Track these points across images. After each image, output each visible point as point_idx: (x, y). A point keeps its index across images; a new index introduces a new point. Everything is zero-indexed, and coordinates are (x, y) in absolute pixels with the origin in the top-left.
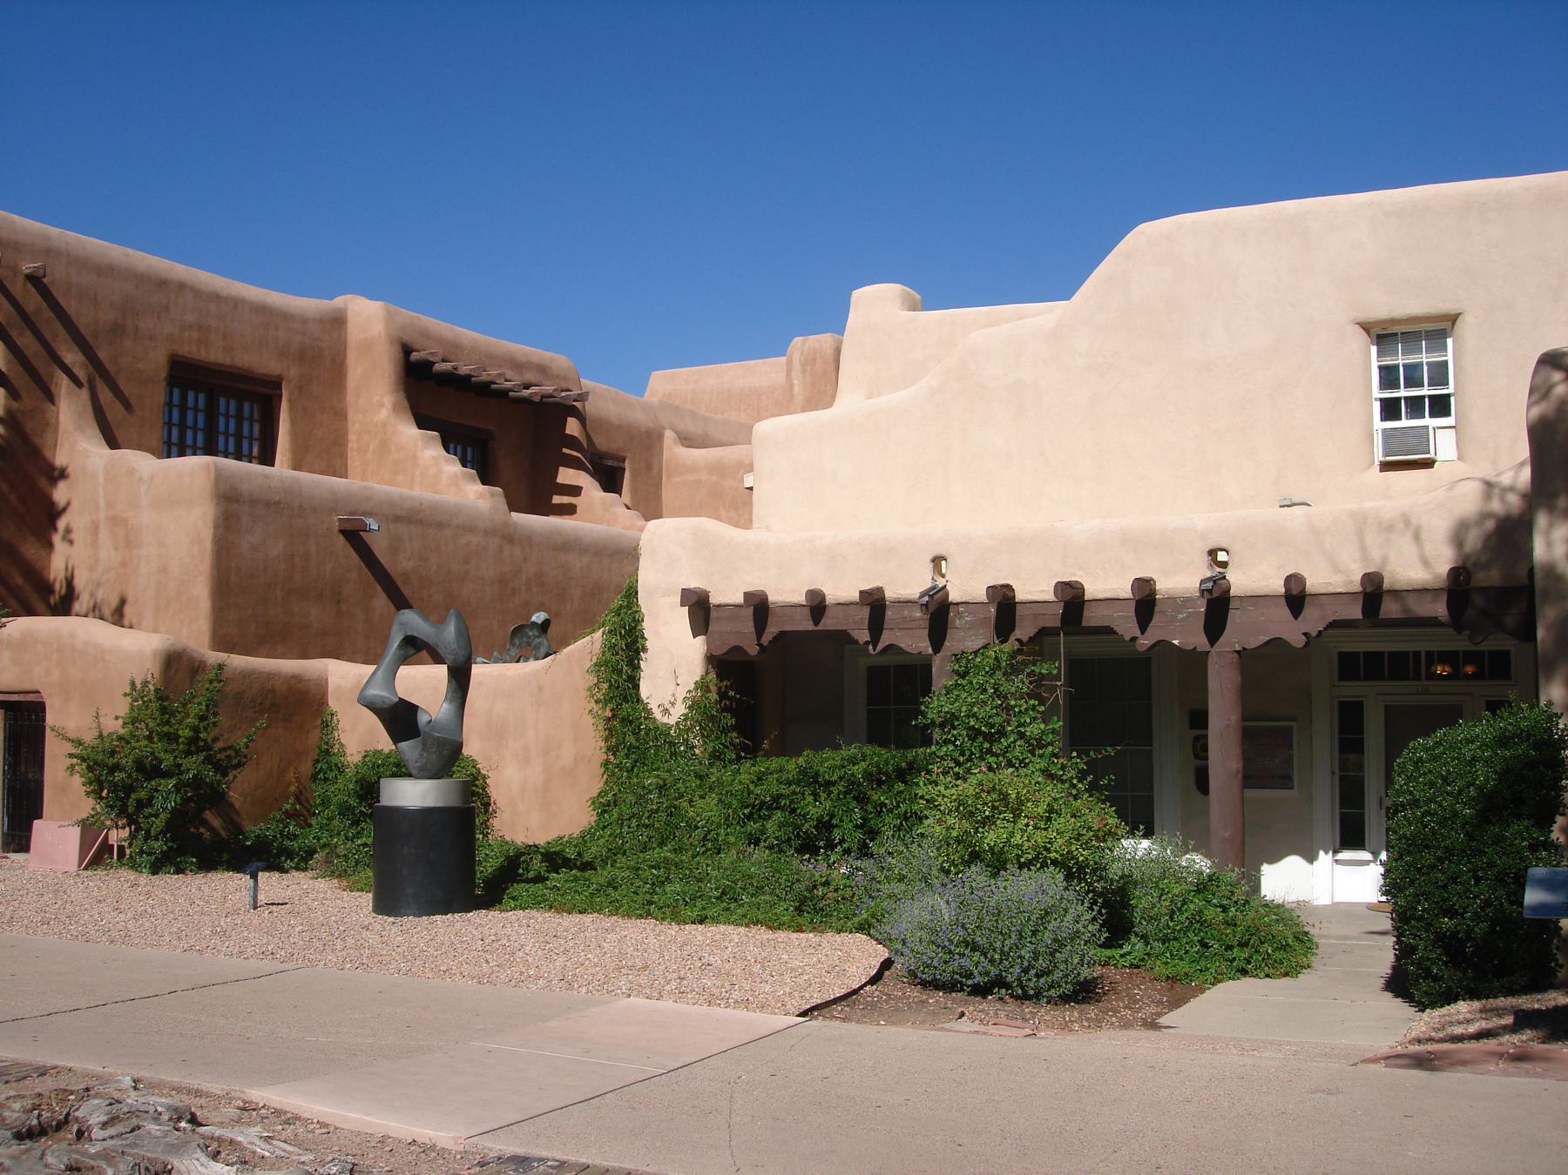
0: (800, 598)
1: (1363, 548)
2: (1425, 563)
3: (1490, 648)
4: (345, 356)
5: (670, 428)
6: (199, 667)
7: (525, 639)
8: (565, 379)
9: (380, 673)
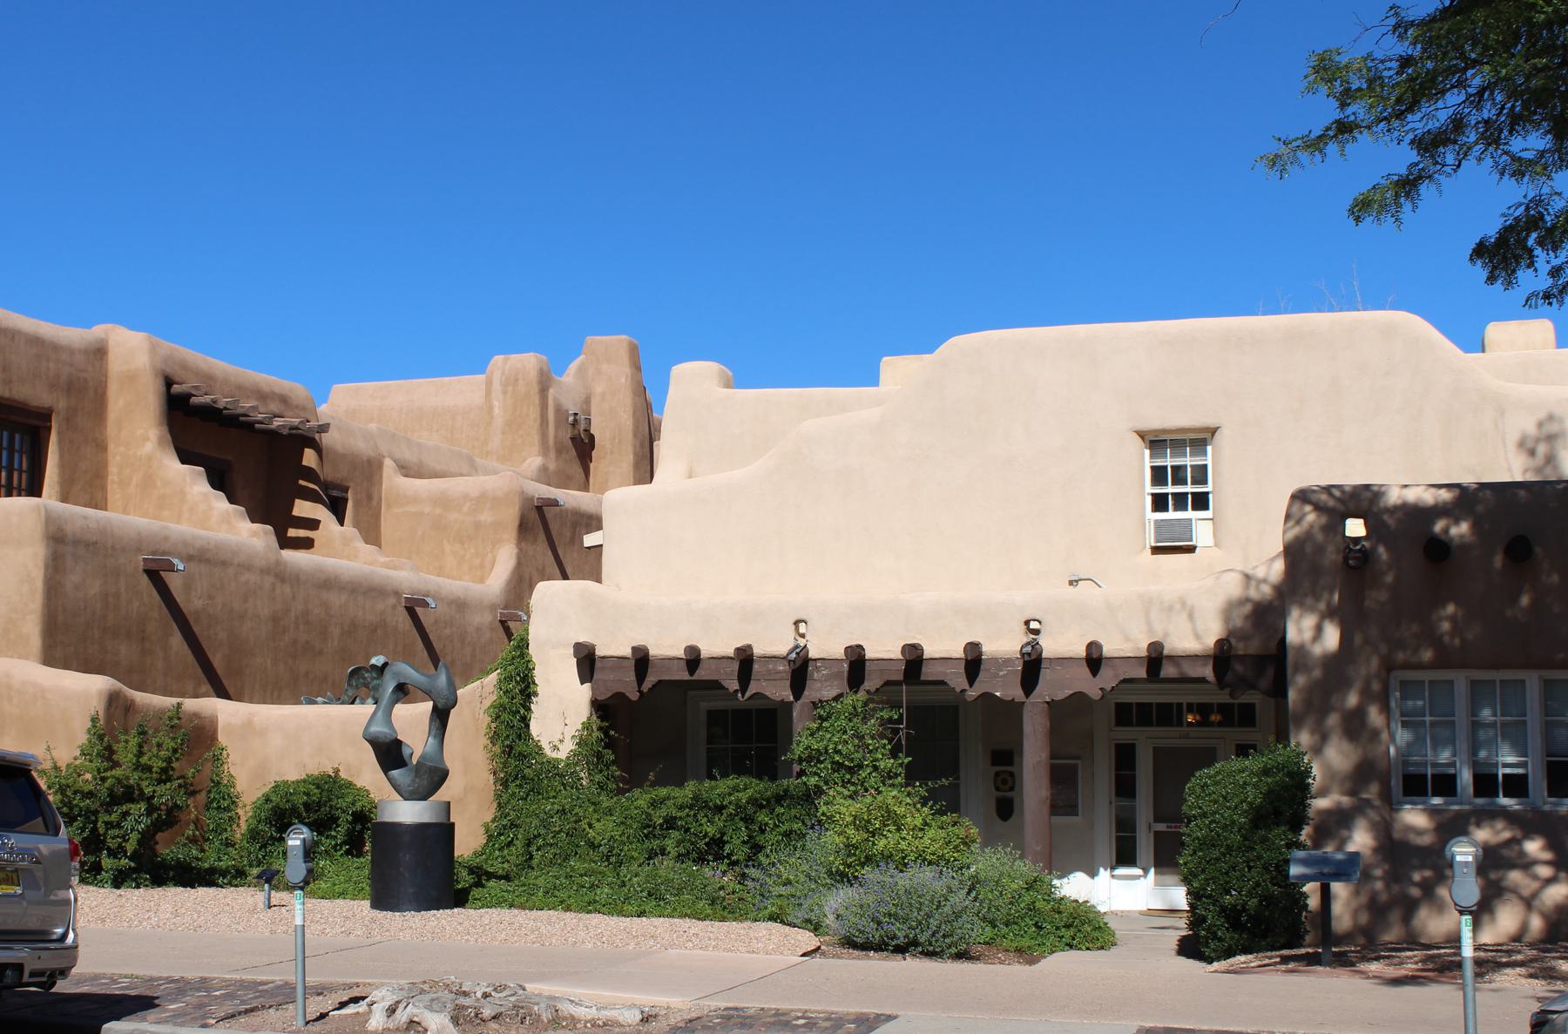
0: (679, 652)
1: (1149, 623)
2: (1197, 637)
3: (1219, 701)
4: (106, 387)
5: (389, 457)
6: (130, 706)
7: (361, 680)
8: (304, 408)
9: (380, 713)
